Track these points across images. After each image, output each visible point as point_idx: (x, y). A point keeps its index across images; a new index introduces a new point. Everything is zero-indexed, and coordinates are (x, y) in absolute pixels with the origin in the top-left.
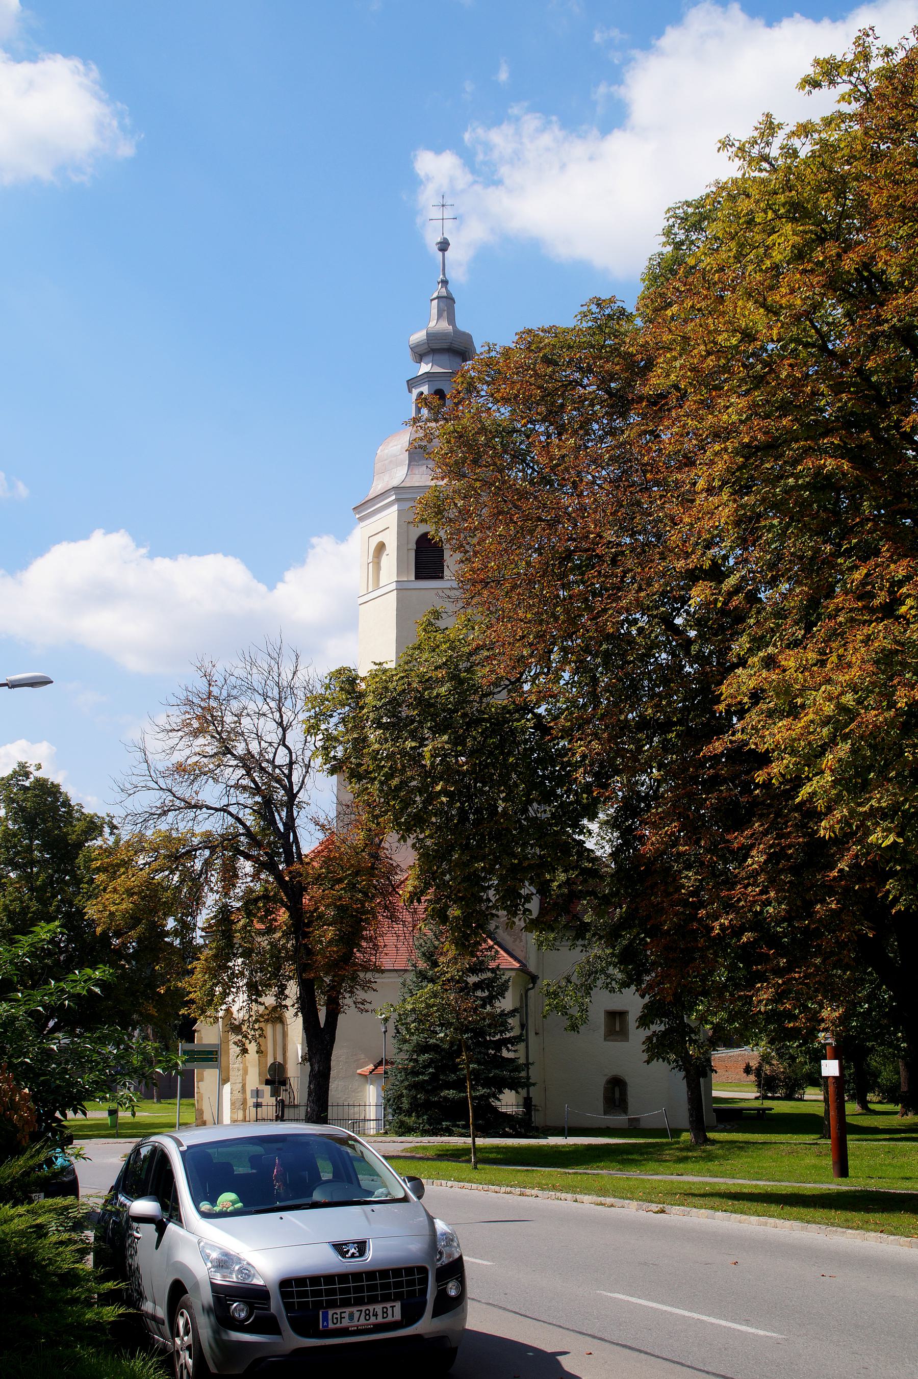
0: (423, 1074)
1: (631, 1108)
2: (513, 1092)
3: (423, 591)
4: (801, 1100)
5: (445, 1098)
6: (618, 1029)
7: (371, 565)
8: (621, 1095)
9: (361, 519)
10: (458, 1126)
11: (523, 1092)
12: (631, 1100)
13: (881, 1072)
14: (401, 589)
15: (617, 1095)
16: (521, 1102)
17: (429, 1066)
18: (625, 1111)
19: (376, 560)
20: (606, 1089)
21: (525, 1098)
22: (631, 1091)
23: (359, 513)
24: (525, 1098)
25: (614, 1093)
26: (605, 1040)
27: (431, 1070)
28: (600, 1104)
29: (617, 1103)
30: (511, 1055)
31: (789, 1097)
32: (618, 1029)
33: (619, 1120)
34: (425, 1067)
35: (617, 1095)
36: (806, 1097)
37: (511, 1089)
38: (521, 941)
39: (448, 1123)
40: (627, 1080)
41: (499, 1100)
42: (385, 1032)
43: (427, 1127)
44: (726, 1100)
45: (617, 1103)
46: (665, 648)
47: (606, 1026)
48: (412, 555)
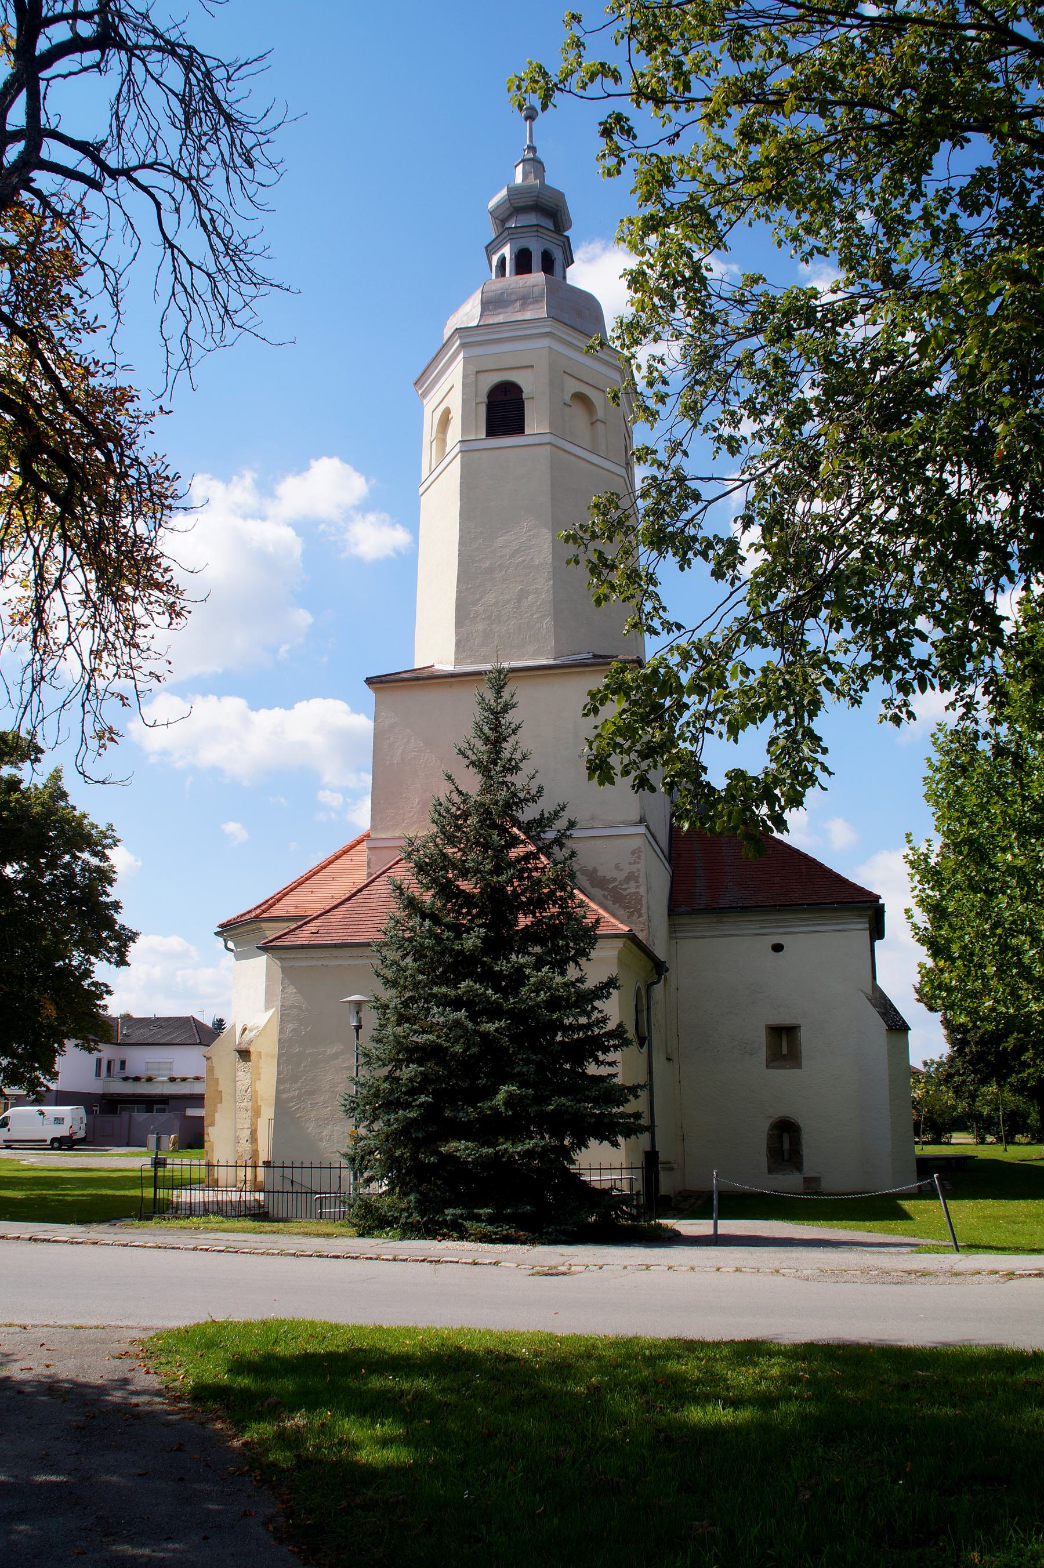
0: (407, 1106)
1: (806, 1164)
2: (606, 1143)
3: (497, 451)
4: (948, 1144)
5: (450, 1158)
6: (785, 1051)
7: (434, 443)
8: (791, 1144)
9: (424, 395)
10: (478, 1218)
11: (643, 1140)
12: (806, 1151)
13: (1030, 1114)
14: (467, 449)
15: (786, 1145)
16: (639, 1160)
17: (421, 1090)
18: (798, 1167)
19: (440, 436)
20: (770, 1137)
21: (646, 1153)
22: (806, 1138)
23: (421, 388)
24: (646, 1153)
25: (781, 1142)
26: (768, 1067)
27: (423, 1098)
28: (762, 1158)
29: (786, 1156)
30: (604, 1071)
31: (936, 1141)
32: (785, 1051)
33: (788, 1182)
34: (413, 1092)
35: (786, 1145)
36: (953, 1141)
37: (601, 1138)
38: (640, 916)
39: (458, 1212)
40: (801, 1122)
41: (573, 1162)
42: (358, 1028)
43: (416, 1217)
44: (137, 1155)
45: (786, 1156)
46: (940, 77)
47: (769, 1047)
48: (483, 410)
